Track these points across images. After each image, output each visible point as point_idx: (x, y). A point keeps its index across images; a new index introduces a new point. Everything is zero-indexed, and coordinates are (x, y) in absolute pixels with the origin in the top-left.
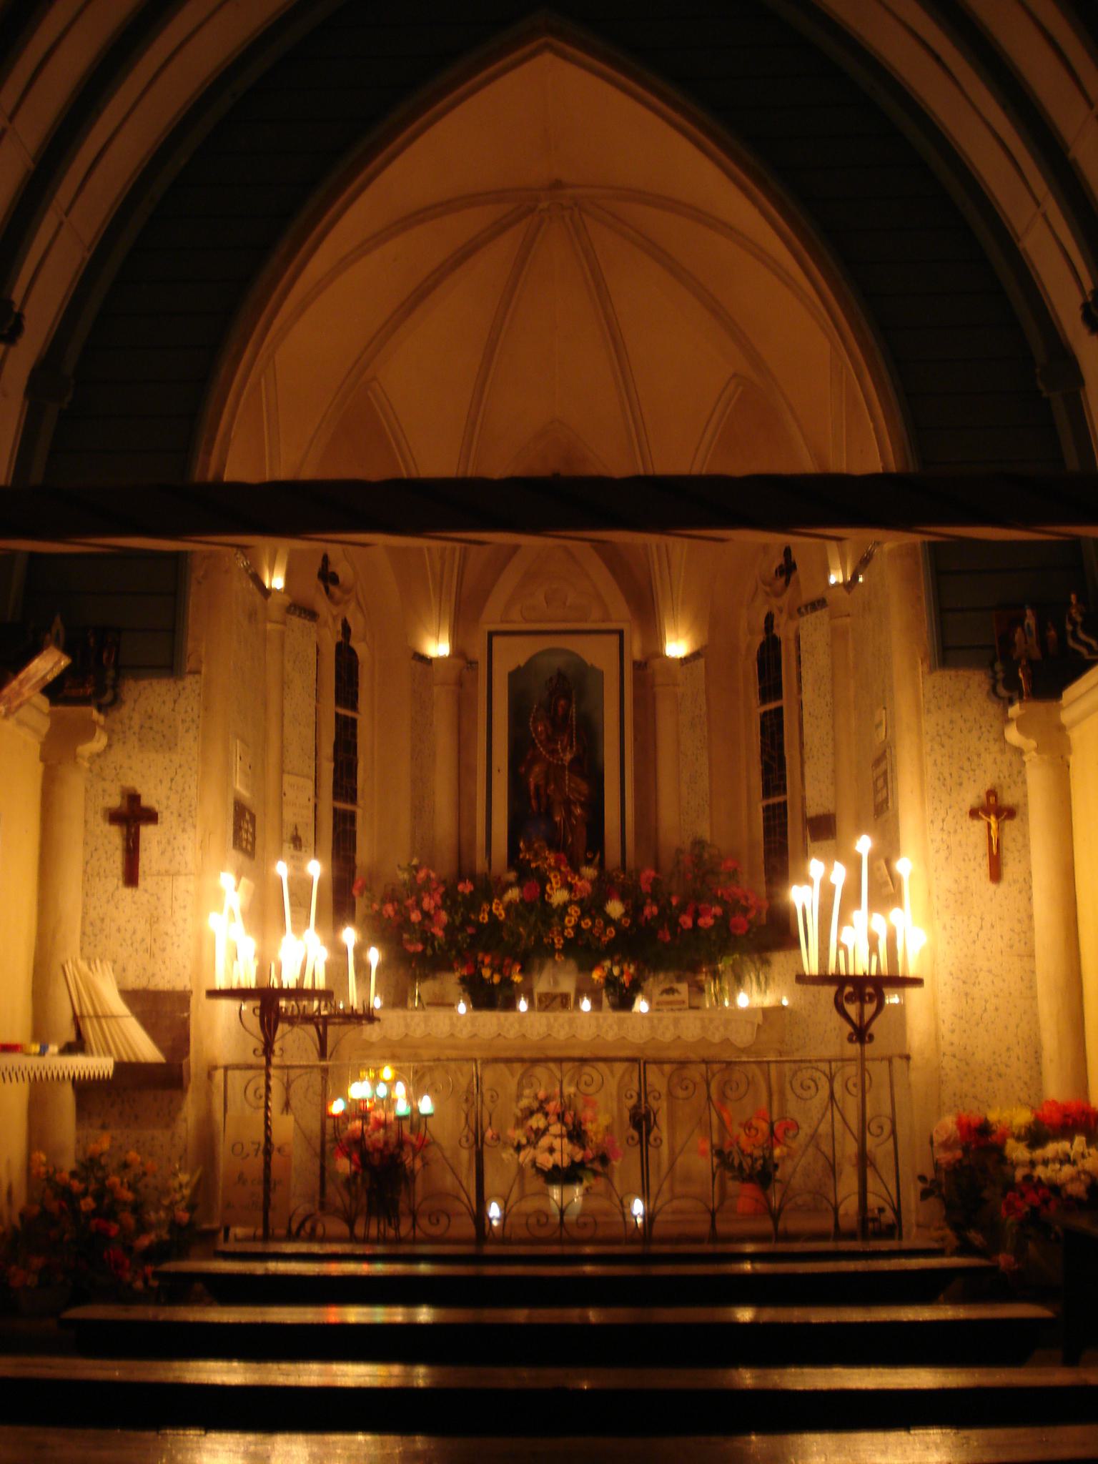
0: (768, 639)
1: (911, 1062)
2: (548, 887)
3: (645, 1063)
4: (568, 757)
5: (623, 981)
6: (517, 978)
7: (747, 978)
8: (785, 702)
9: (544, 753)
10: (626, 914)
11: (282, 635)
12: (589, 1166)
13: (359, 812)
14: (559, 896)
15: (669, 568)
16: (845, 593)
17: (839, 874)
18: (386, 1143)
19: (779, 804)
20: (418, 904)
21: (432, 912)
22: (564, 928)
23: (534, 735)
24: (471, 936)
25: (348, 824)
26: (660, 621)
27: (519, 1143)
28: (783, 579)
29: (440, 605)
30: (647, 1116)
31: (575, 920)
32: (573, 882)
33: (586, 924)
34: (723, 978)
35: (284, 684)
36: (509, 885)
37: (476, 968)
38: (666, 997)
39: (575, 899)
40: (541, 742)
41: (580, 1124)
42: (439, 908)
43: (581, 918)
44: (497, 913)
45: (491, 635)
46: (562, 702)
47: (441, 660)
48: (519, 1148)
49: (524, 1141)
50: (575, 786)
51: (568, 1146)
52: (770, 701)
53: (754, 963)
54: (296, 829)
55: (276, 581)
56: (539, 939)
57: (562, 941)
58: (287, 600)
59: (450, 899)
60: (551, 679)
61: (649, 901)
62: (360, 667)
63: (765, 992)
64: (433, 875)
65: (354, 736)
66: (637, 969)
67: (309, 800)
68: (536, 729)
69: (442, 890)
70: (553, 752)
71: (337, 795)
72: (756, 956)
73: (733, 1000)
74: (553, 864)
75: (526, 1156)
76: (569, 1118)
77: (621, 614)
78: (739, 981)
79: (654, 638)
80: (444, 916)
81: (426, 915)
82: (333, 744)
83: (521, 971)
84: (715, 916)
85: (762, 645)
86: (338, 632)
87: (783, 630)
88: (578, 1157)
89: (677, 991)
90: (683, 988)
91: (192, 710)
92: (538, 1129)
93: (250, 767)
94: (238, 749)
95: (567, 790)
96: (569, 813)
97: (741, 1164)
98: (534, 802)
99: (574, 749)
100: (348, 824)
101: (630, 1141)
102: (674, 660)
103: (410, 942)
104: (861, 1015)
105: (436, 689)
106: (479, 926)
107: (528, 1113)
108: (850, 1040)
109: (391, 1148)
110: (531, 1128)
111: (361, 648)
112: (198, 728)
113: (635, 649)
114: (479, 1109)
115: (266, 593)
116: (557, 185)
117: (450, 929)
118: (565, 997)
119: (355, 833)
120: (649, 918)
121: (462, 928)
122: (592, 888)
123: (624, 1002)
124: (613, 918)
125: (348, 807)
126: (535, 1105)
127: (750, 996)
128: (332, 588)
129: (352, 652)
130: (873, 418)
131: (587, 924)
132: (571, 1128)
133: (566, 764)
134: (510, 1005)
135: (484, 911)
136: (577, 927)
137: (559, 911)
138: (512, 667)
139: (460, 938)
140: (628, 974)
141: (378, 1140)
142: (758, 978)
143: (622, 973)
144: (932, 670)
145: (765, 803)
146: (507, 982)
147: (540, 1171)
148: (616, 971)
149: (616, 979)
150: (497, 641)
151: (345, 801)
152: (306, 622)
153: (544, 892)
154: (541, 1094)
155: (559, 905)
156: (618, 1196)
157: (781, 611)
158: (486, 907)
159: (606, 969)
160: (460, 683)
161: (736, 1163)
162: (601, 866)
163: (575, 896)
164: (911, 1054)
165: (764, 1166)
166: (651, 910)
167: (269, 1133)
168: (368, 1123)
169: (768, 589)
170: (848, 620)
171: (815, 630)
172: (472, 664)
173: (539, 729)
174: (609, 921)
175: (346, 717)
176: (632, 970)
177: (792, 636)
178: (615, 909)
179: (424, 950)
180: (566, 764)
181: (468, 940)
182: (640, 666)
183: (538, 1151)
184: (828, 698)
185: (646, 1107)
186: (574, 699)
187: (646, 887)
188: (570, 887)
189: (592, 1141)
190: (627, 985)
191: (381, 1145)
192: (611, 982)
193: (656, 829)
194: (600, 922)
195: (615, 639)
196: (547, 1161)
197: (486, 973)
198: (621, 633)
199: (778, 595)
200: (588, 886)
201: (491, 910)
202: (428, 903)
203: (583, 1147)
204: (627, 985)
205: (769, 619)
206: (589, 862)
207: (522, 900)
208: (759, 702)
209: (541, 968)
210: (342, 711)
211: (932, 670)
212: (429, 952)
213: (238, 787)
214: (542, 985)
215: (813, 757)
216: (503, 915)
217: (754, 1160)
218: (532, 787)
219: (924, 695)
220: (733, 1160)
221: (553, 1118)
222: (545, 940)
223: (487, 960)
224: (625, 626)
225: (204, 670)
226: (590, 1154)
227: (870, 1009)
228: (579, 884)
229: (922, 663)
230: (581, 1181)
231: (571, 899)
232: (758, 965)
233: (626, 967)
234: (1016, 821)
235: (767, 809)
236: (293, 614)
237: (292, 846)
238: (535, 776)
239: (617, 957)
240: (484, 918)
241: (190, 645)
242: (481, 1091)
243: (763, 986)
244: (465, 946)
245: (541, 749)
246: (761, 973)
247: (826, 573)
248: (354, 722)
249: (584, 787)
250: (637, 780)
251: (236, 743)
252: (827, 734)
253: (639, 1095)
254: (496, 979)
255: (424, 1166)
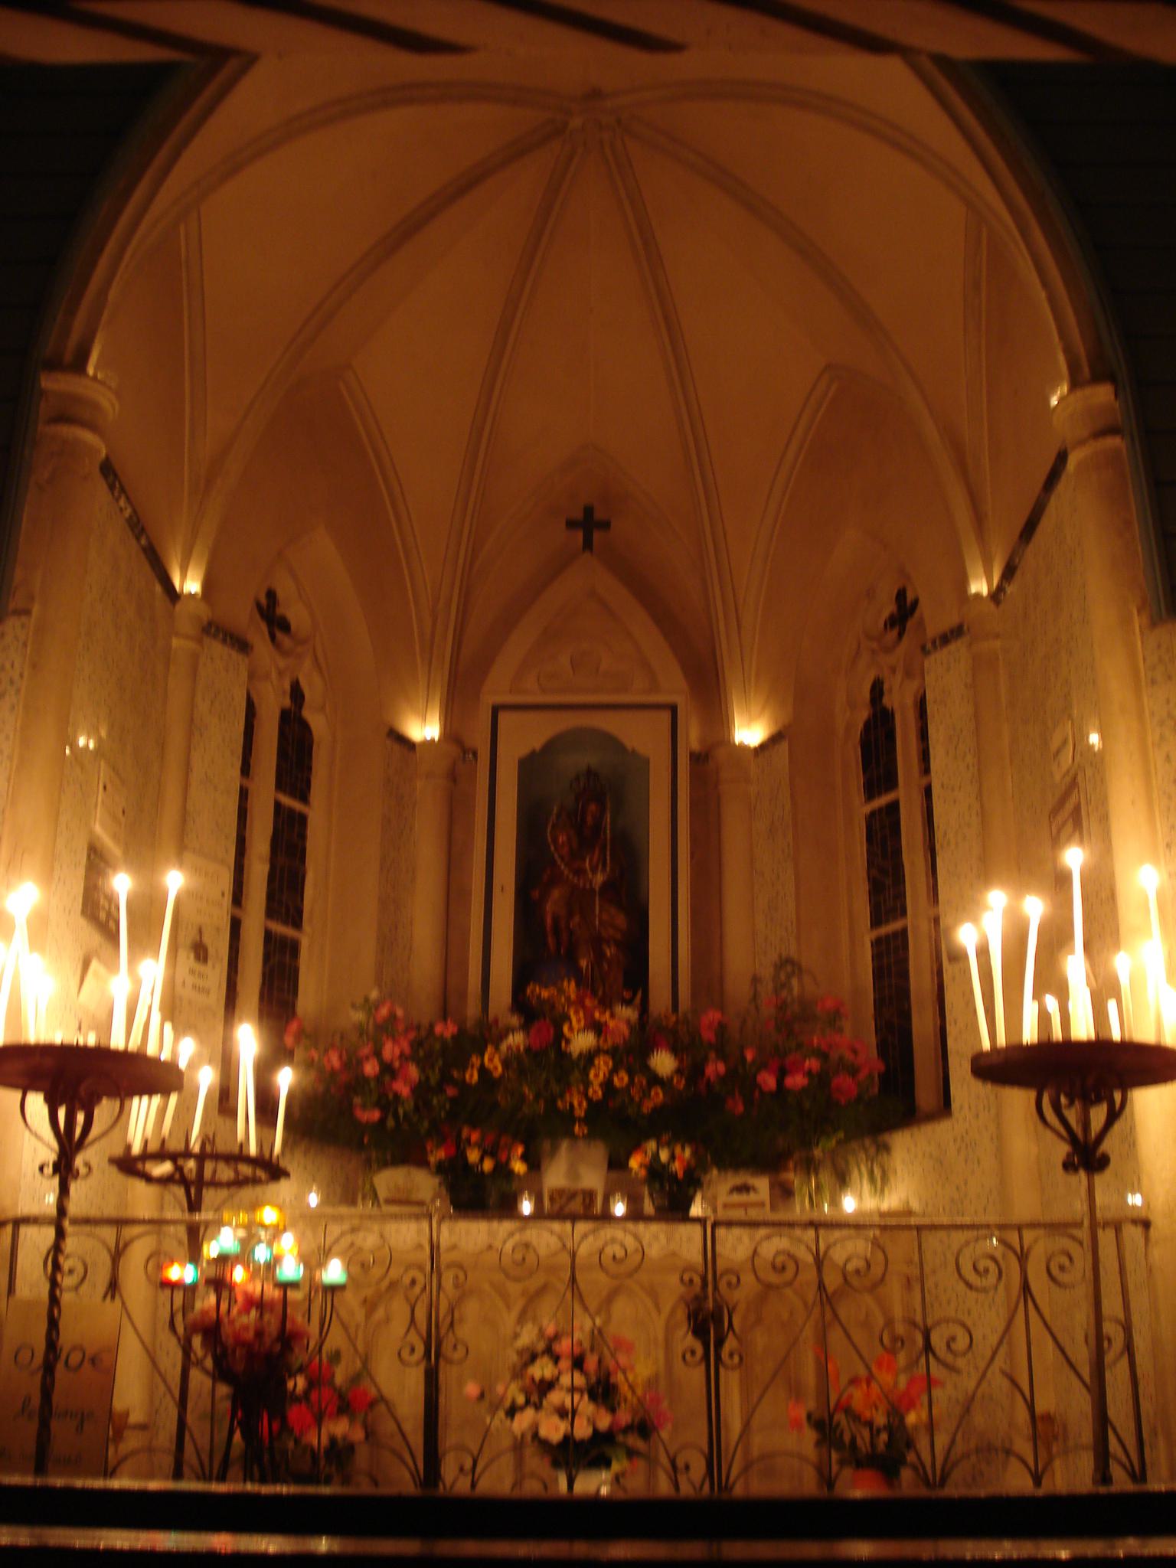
0: (875, 715)
1: (1152, 1230)
2: (566, 1029)
3: (714, 1225)
4: (599, 878)
5: (674, 1169)
6: (519, 1167)
7: (855, 1174)
8: (906, 794)
9: (566, 872)
10: (679, 1071)
11: (195, 658)
12: (620, 1438)
13: (305, 943)
14: (581, 1041)
15: (739, 633)
16: (992, 606)
17: (1035, 907)
18: (259, 1333)
19: (895, 934)
20: (378, 1053)
21: (397, 1064)
22: (587, 1084)
23: (552, 848)
24: (452, 1100)
25: (288, 957)
26: (725, 690)
27: (513, 1402)
28: (895, 633)
29: (428, 692)
30: (716, 1316)
31: (604, 1075)
32: (603, 1020)
33: (621, 1080)
34: (821, 1170)
35: (193, 726)
36: (509, 1030)
37: (458, 1147)
38: (736, 1198)
39: (605, 1048)
40: (562, 858)
41: (608, 1375)
42: (407, 1059)
43: (614, 1071)
44: (491, 1067)
45: (496, 711)
46: (593, 807)
47: (428, 744)
48: (512, 1411)
49: (521, 1399)
50: (611, 919)
51: (586, 1407)
52: (880, 794)
53: (866, 1151)
54: (200, 932)
55: (191, 585)
56: (551, 1102)
57: (585, 1104)
58: (204, 612)
59: (423, 1049)
60: (577, 778)
61: (712, 1055)
62: (315, 747)
63: (882, 1191)
64: (400, 1013)
65: (303, 837)
66: (694, 1153)
67: (223, 894)
68: (555, 840)
69: (412, 1035)
70: (580, 872)
71: (271, 913)
72: (867, 1142)
73: (835, 1203)
74: (573, 996)
75: (523, 1421)
76: (591, 1362)
77: (674, 687)
78: (842, 1180)
79: (719, 721)
80: (413, 1072)
81: (387, 1069)
82: (269, 839)
83: (524, 1158)
84: (809, 1074)
85: (867, 725)
86: (284, 692)
87: (900, 699)
88: (604, 1422)
89: (755, 1189)
90: (762, 1185)
91: (12, 666)
92: (542, 1380)
93: (124, 812)
94: (102, 775)
95: (597, 923)
96: (599, 956)
97: (853, 1440)
98: (550, 940)
99: (608, 869)
100: (288, 957)
101: (688, 1356)
102: (743, 748)
103: (364, 1107)
104: (1086, 1124)
105: (419, 784)
106: (463, 1085)
107: (526, 1357)
108: (1068, 1166)
109: (268, 1341)
110: (533, 1379)
111: (316, 721)
112: (18, 691)
113: (692, 736)
114: (434, 1298)
115: (173, 595)
116: (595, 94)
117: (421, 1091)
118: (589, 1195)
119: (296, 971)
120: (712, 1079)
121: (440, 1089)
122: (631, 1033)
123: (675, 1209)
124: (660, 1075)
125: (288, 931)
126: (541, 1346)
127: (860, 1197)
128: (279, 635)
129: (305, 726)
130: (1045, 284)
131: (622, 1079)
132: (593, 1379)
133: (597, 889)
134: (508, 1208)
135: (473, 1066)
136: (608, 1085)
137: (582, 1063)
138: (523, 751)
139: (435, 1101)
140: (681, 1159)
141: (246, 1328)
142: (871, 1173)
143: (673, 1157)
144: (1154, 624)
145: (875, 934)
146: (503, 1170)
147: (544, 1444)
148: (664, 1156)
149: (665, 1167)
150: (505, 719)
151: (285, 922)
152: (234, 654)
153: (559, 1036)
154: (550, 1330)
155: (581, 1054)
156: (667, 1452)
157: (893, 670)
158: (475, 1060)
159: (649, 1153)
160: (453, 776)
161: (847, 1438)
162: (644, 1009)
163: (605, 1041)
164: (1152, 1218)
165: (889, 1444)
166: (715, 1068)
167: (56, 1312)
168: (232, 1300)
169: (875, 645)
170: (998, 644)
171: (948, 670)
172: (467, 753)
173: (560, 840)
174: (655, 1079)
175: (291, 811)
176: (688, 1153)
177: (909, 701)
178: (663, 1062)
179: (383, 1120)
180: (597, 889)
181: (448, 1106)
182: (699, 759)
183: (542, 1414)
184: (969, 759)
185: (715, 1300)
186: (609, 805)
187: (708, 1035)
188: (598, 1028)
189: (626, 1400)
190: (680, 1175)
191: (250, 1335)
192: (656, 1172)
193: (721, 979)
194: (641, 1080)
195: (665, 717)
196: (554, 1430)
197: (473, 1156)
198: (673, 709)
199: (888, 650)
200: (624, 1029)
201: (482, 1064)
202: (389, 1051)
203: (613, 1410)
204: (680, 1175)
205: (877, 690)
206: (628, 1003)
207: (528, 1049)
208: (863, 800)
209: (555, 1149)
210: (287, 801)
211: (1154, 624)
212: (391, 1123)
213: (98, 829)
214: (555, 1177)
215: (949, 843)
216: (500, 1069)
217: (874, 1433)
218: (549, 921)
219: (1144, 660)
220: (842, 1433)
221: (565, 1364)
222: (560, 1104)
223: (475, 1137)
224: (680, 700)
225: (36, 609)
226: (624, 1417)
227: (1098, 1115)
228: (611, 1024)
229: (1139, 612)
230: (607, 1464)
231: (598, 1047)
232: (872, 1150)
233: (678, 1150)
234: (1108, 1173)
235: (877, 943)
236: (215, 636)
237: (192, 956)
238: (554, 902)
239: (665, 1137)
240: (473, 1076)
241: (19, 574)
242: (438, 1267)
243: (881, 1182)
244: (443, 1114)
245: (563, 867)
246: (875, 1165)
247: (963, 583)
248: (303, 820)
249: (621, 920)
250: (694, 805)
251: (100, 765)
252: (970, 807)
253: (704, 1279)
254: (488, 1165)
255: (367, 1436)
